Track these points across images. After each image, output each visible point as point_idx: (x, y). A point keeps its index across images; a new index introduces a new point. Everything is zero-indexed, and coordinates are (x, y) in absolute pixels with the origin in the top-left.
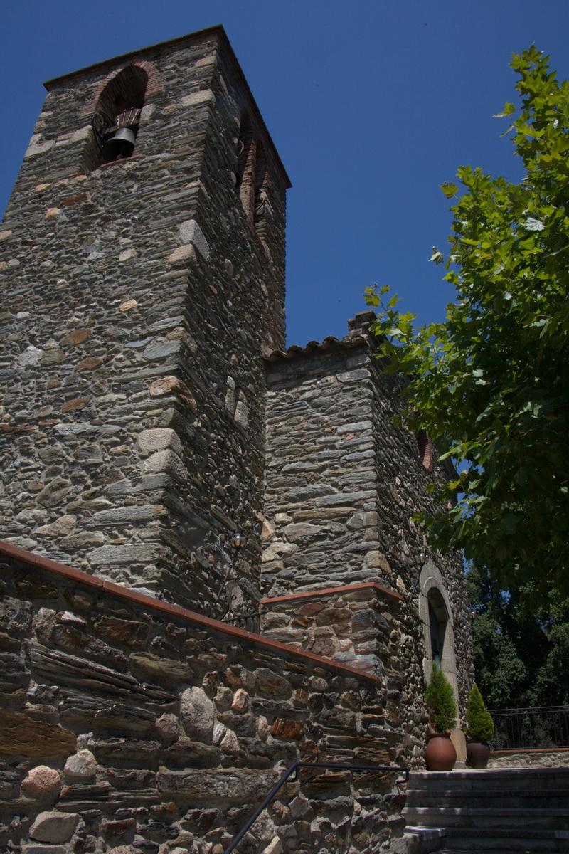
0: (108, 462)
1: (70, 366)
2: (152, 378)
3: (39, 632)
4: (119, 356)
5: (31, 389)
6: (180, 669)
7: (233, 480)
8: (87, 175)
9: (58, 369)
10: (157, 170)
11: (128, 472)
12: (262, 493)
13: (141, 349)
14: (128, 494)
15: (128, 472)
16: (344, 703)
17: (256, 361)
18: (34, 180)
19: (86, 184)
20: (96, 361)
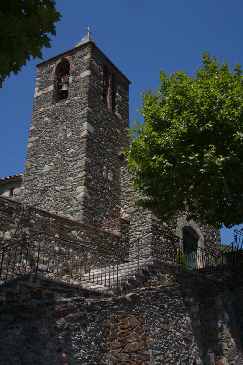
0: (69, 196)
1: (57, 170)
2: (79, 172)
3: (51, 221)
4: (70, 166)
5: (48, 178)
6: (71, 228)
7: (107, 197)
8: (55, 105)
9: (54, 171)
10: (75, 104)
11: (75, 198)
12: (120, 200)
13: (75, 164)
14: (75, 204)
15: (75, 198)
16: (109, 239)
17: (115, 158)
18: (38, 107)
19: (55, 108)
20: (64, 168)
